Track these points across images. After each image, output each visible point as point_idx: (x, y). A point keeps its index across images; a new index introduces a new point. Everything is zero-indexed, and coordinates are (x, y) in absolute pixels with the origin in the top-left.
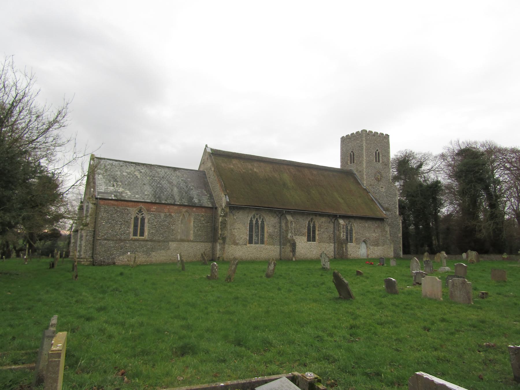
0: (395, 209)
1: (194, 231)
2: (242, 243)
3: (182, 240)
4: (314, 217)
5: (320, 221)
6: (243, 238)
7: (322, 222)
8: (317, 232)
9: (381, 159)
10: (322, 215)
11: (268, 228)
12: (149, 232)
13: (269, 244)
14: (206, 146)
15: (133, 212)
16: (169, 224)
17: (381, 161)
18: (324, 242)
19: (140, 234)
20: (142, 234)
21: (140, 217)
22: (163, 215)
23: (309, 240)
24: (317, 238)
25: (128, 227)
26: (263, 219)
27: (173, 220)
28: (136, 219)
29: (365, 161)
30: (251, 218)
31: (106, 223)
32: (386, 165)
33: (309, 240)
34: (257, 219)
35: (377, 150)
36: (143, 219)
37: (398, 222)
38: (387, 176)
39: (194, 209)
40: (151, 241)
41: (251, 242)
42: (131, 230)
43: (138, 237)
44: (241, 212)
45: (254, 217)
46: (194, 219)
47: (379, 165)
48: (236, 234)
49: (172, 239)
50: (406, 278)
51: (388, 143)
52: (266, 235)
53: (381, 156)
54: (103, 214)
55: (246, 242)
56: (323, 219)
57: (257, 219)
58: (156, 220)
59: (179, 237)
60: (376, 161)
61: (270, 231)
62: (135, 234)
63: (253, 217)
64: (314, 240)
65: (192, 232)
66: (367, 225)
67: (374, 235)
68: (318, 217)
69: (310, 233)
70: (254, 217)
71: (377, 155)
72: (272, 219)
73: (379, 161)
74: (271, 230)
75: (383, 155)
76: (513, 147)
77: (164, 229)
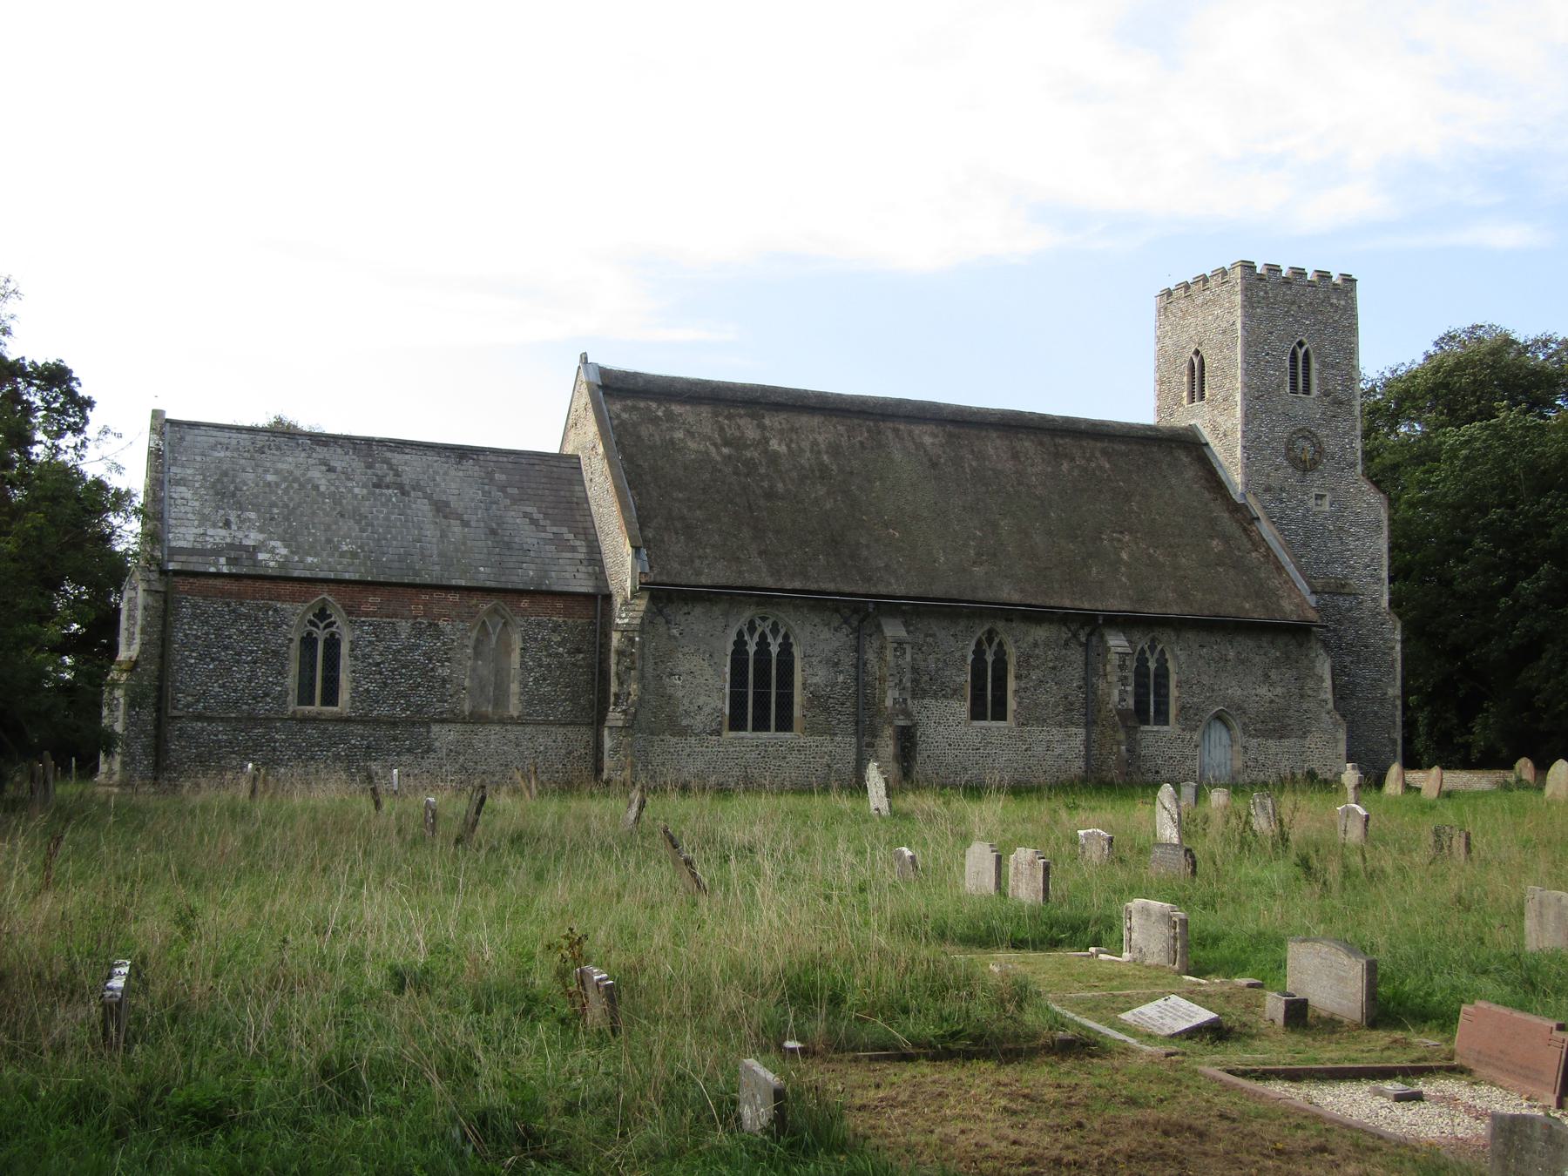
1: (524, 685)
2: (701, 726)
3: (477, 719)
4: (1000, 625)
5: (1016, 642)
6: (707, 710)
7: (1036, 645)
8: (1012, 684)
9: (1314, 381)
10: (1034, 615)
12: (355, 690)
13: (811, 730)
15: (296, 615)
17: (1315, 391)
18: (1041, 721)
20: (330, 697)
21: (321, 635)
22: (404, 627)
23: (977, 713)
24: (1012, 704)
26: (786, 637)
27: (444, 644)
28: (308, 642)
30: (740, 634)
31: (201, 658)
33: (977, 713)
34: (763, 636)
35: (1301, 344)
36: (333, 644)
37: (1386, 640)
39: (525, 603)
41: (737, 723)
43: (316, 708)
44: (698, 610)
46: (524, 641)
48: (680, 694)
49: (441, 713)
51: (1350, 311)
52: (798, 698)
53: (1314, 365)
54: (186, 630)
55: (721, 723)
56: (1040, 633)
57: (763, 636)
60: (1294, 389)
61: (816, 680)
62: (306, 697)
63: (745, 628)
64: (1000, 714)
65: (515, 687)
66: (1232, 654)
67: (1263, 690)
68: (1018, 627)
70: (752, 628)
72: (826, 634)
73: (1307, 391)
74: (820, 677)
75: (1324, 365)
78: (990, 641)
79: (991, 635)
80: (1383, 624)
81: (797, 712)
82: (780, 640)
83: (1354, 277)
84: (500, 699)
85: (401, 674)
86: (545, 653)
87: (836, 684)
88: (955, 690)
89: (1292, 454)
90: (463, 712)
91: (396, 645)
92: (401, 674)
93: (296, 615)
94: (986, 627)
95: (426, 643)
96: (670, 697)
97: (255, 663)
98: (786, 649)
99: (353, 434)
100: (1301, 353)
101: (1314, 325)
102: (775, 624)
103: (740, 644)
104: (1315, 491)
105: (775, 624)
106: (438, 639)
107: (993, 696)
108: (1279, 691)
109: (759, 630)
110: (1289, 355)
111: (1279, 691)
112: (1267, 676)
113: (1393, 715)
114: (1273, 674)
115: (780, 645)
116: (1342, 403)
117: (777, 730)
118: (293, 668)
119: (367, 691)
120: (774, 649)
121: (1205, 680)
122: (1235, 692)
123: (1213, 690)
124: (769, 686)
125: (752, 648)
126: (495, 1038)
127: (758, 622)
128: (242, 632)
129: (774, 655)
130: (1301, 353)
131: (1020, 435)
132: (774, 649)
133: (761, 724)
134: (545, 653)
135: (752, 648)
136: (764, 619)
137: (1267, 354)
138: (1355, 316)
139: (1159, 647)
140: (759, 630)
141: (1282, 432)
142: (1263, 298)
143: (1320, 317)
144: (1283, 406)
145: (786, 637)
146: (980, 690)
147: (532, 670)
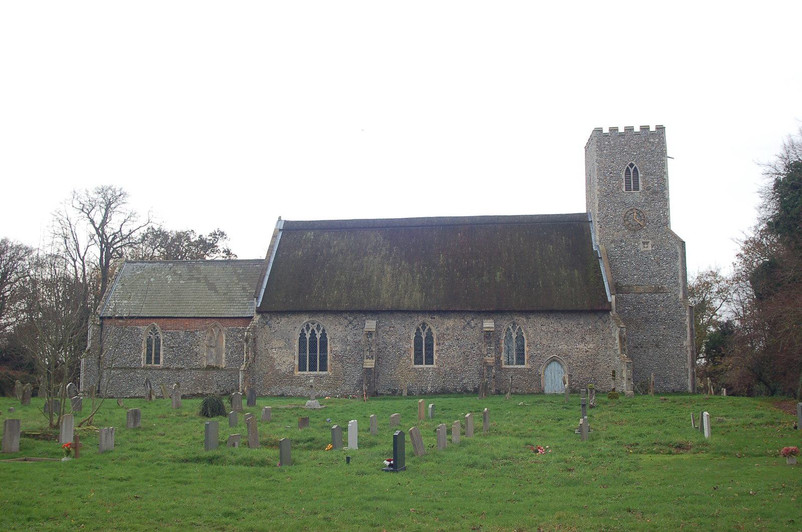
0: (676, 288)
1: (227, 354)
2: (285, 369)
4: (428, 319)
6: (287, 363)
7: (448, 329)
8: (435, 348)
9: (640, 183)
11: (333, 345)
12: (165, 358)
14: (280, 218)
16: (191, 345)
17: (641, 189)
19: (425, 362)
20: (157, 360)
24: (435, 357)
25: (139, 352)
26: (324, 331)
27: (196, 339)
28: (149, 342)
29: (598, 193)
30: (303, 330)
32: (655, 193)
34: (313, 331)
35: (632, 165)
37: (682, 316)
38: (658, 216)
40: (168, 369)
42: (143, 355)
45: (308, 328)
46: (227, 337)
47: (637, 196)
48: (275, 356)
49: (196, 366)
50: (448, 413)
55: (294, 368)
57: (313, 331)
58: (173, 341)
59: (205, 364)
61: (336, 349)
62: (149, 360)
63: (305, 328)
65: (224, 355)
67: (581, 346)
69: (421, 350)
70: (308, 328)
71: (632, 175)
74: (338, 348)
75: (646, 174)
76: (770, 182)
77: (184, 353)
78: (424, 328)
79: (424, 325)
80: (680, 308)
81: (329, 363)
82: (321, 332)
83: (664, 126)
84: (219, 361)
85: (181, 351)
86: (235, 341)
87: (346, 350)
88: (405, 351)
89: (627, 223)
90: (203, 365)
91: (179, 340)
92: (181, 351)
93: (144, 329)
94: (421, 321)
95: (190, 339)
96: (272, 358)
97: (131, 349)
98: (324, 335)
99: (250, 259)
100: (632, 170)
101: (639, 154)
102: (318, 326)
103: (303, 335)
104: (642, 240)
105: (318, 326)
106: (194, 337)
107: (426, 353)
108: (591, 346)
109: (311, 328)
110: (624, 172)
111: (591, 346)
112: (583, 339)
113: (686, 356)
114: (587, 338)
115: (321, 334)
116: (657, 192)
117: (309, 371)
118: (144, 351)
119: (169, 358)
120: (318, 336)
121: (544, 342)
122: (563, 347)
123: (550, 347)
124: (316, 352)
125: (308, 336)
126: (532, 500)
127: (310, 325)
128: (126, 337)
129: (318, 339)
130: (632, 170)
131: (764, 225)
132: (318, 336)
133: (313, 368)
134: (235, 341)
135: (308, 336)
136: (313, 324)
137: (611, 173)
138: (665, 147)
139: (427, 328)
140: (311, 328)
141: (621, 211)
142: (608, 145)
143: (643, 150)
144: (621, 198)
145: (324, 331)
146: (419, 351)
147: (230, 349)
